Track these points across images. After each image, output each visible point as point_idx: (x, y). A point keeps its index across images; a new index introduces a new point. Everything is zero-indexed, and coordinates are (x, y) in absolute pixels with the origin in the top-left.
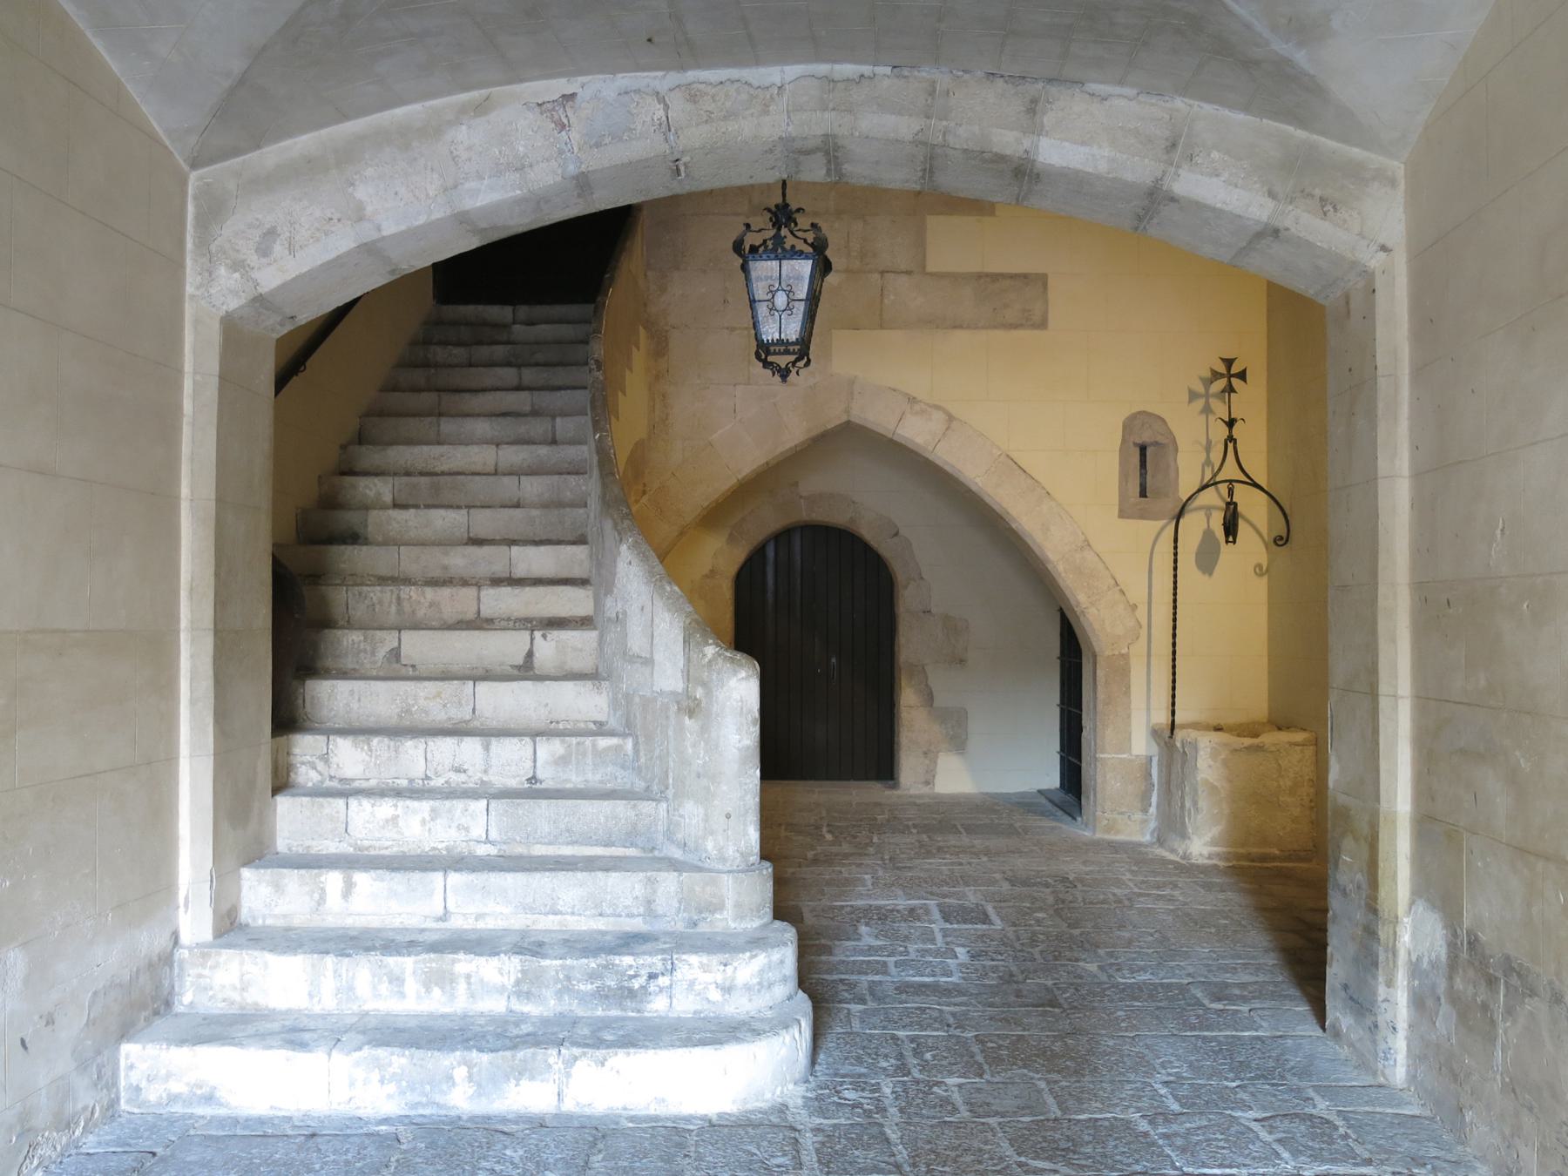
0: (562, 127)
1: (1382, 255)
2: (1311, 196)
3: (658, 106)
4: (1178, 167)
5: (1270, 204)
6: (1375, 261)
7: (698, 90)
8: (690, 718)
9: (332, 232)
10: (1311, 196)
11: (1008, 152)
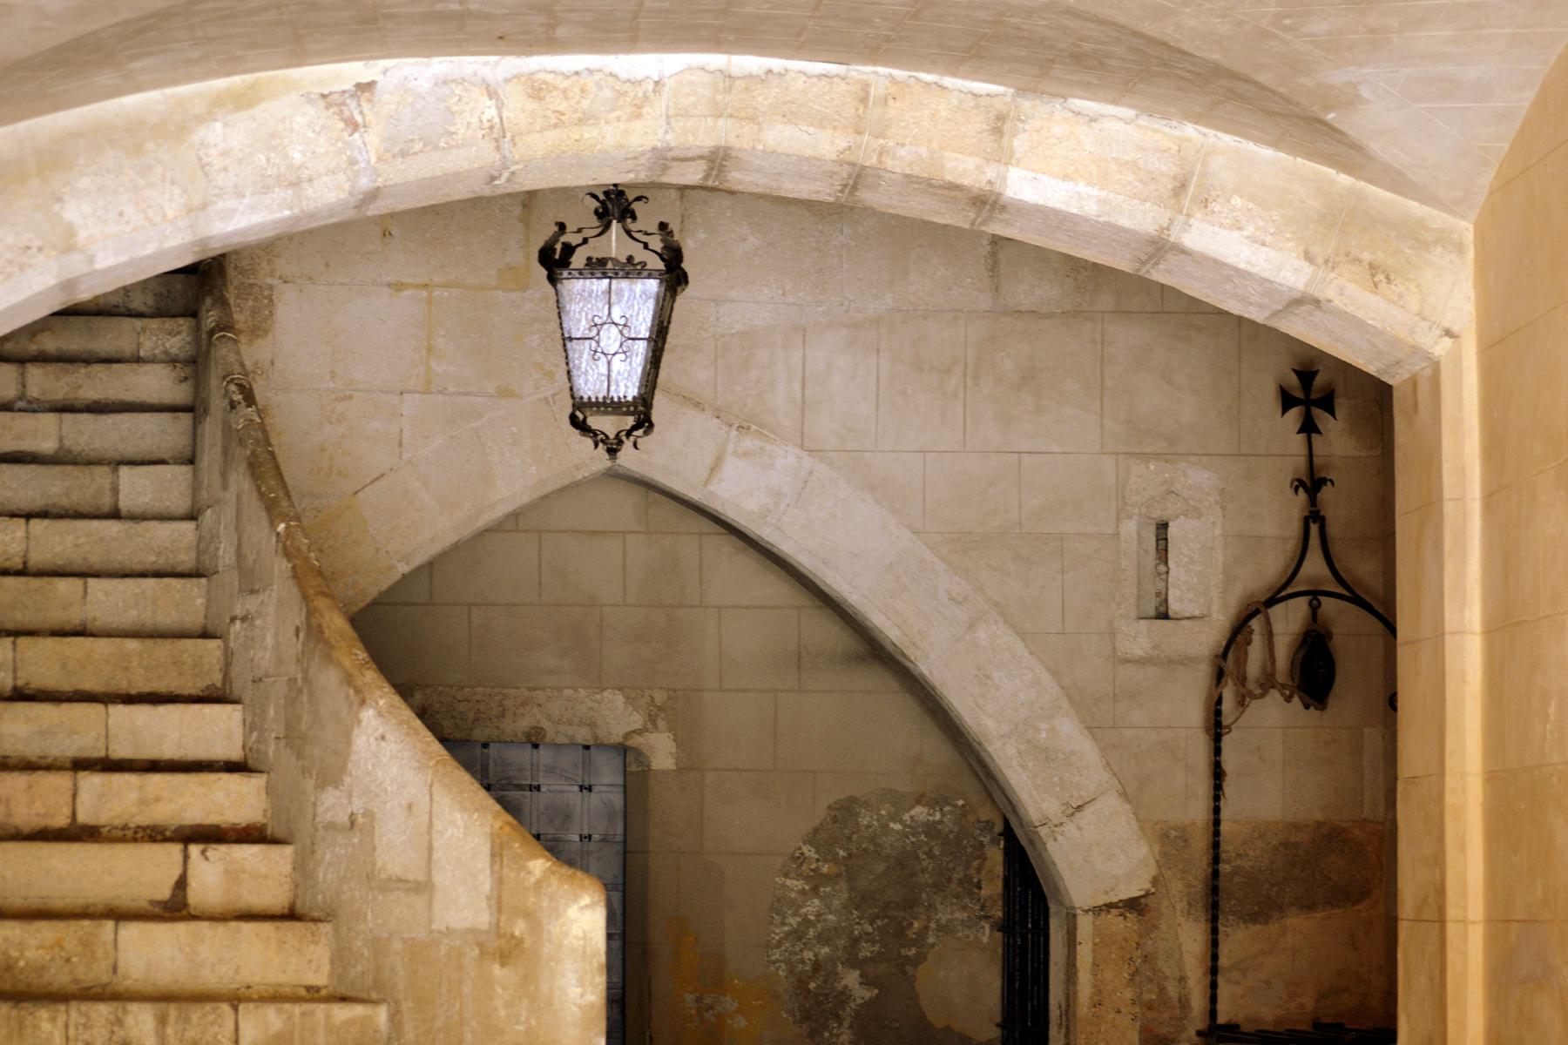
0: (354, 126)
1: (1448, 341)
2: (1357, 261)
3: (489, 103)
4: (1189, 216)
5: (1308, 269)
6: (1442, 348)
7: (545, 82)
8: (503, 965)
9: (30, 266)
10: (1357, 261)
11: (966, 182)
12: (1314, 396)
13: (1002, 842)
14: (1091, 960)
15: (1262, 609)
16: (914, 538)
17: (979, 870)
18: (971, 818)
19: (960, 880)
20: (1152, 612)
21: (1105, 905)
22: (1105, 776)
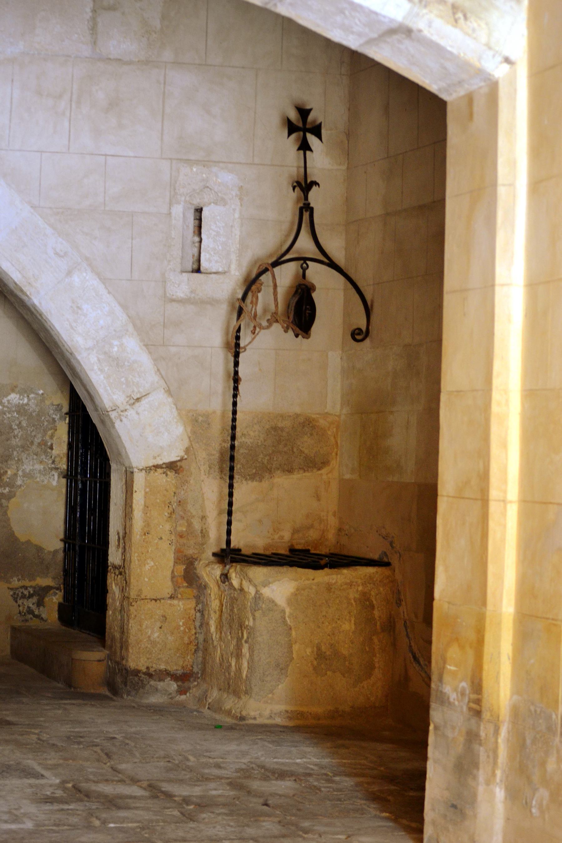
1: (506, 67)
12: (307, 126)
13: (67, 419)
14: (143, 502)
15: (270, 268)
16: (32, 211)
17: (52, 437)
18: (48, 403)
19: (39, 444)
20: (190, 269)
21: (154, 466)
22: (156, 378)
